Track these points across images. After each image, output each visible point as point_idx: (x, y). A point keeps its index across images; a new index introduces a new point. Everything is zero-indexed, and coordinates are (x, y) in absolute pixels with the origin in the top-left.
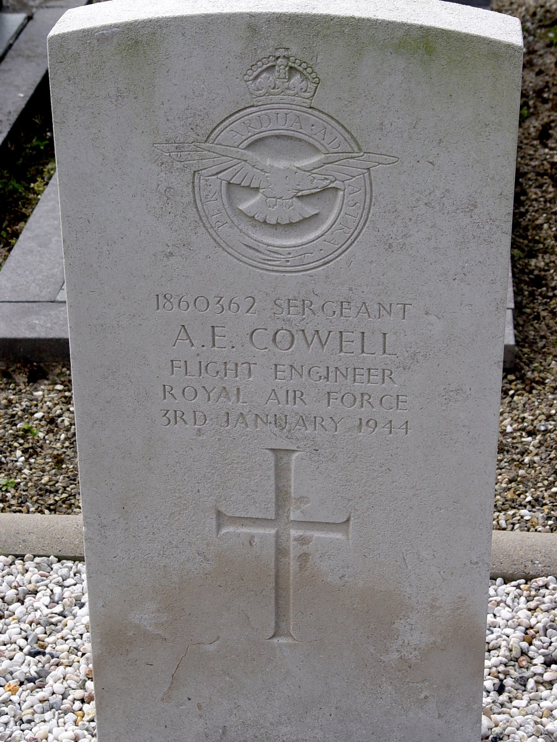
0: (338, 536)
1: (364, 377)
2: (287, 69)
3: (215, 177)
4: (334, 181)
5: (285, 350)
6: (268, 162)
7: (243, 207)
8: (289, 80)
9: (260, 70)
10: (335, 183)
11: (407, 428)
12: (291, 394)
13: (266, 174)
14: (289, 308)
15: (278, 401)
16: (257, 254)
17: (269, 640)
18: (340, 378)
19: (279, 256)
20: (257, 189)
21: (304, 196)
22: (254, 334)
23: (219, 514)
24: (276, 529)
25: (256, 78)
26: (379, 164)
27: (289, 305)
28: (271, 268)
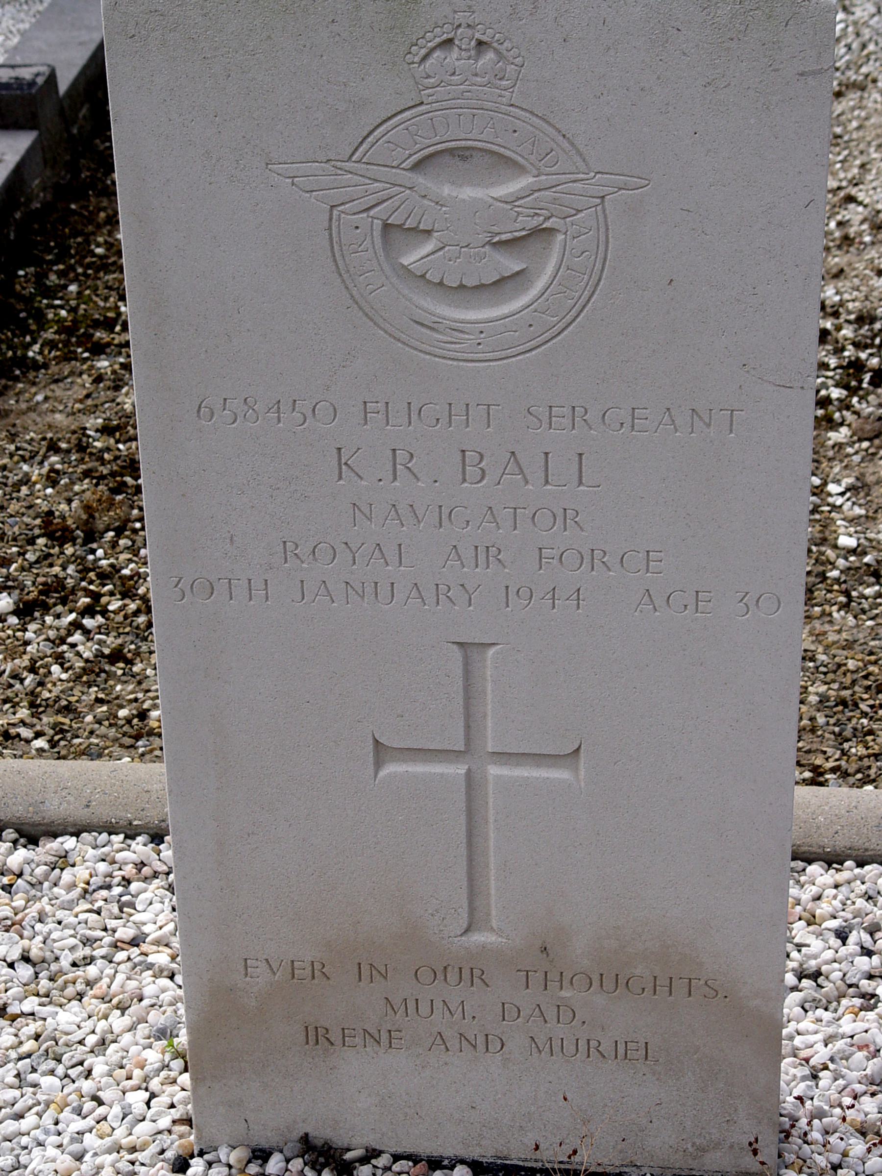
3: (365, 215)
4: (549, 218)
6: (446, 190)
7: (405, 261)
8: (476, 61)
10: (551, 220)
11: (578, 599)
13: (444, 209)
14: (550, 418)
19: (467, 336)
20: (428, 232)
23: (376, 742)
24: (467, 767)
26: (620, 189)
27: (550, 413)
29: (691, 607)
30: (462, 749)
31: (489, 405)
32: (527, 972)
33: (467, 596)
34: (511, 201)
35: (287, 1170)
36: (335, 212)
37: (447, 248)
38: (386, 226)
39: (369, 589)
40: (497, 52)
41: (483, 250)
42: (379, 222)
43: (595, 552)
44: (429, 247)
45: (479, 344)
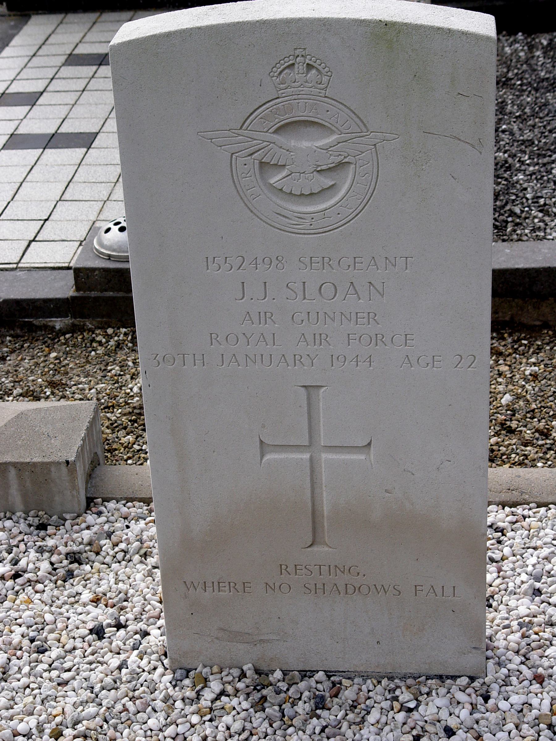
0: (363, 457)
1: (365, 320)
2: (305, 65)
3: (249, 158)
5: (332, 299)
6: (293, 143)
7: (272, 181)
9: (282, 67)
11: (370, 362)
12: (317, 337)
13: (292, 153)
15: (307, 343)
16: (287, 220)
17: (309, 549)
18: (345, 321)
19: (304, 221)
20: (284, 165)
21: (323, 170)
22: (323, 287)
23: (261, 442)
25: (281, 73)
28: (296, 231)
29: (430, 365)
30: (307, 443)
31: (406, 258)
32: (320, 566)
33: (311, 361)
34: (326, 149)
35: (510, 711)
36: (234, 157)
37: (293, 174)
38: (261, 163)
39: (258, 358)
40: (318, 70)
41: (312, 175)
42: (258, 161)
43: (378, 335)
44: (285, 173)
45: (311, 225)
